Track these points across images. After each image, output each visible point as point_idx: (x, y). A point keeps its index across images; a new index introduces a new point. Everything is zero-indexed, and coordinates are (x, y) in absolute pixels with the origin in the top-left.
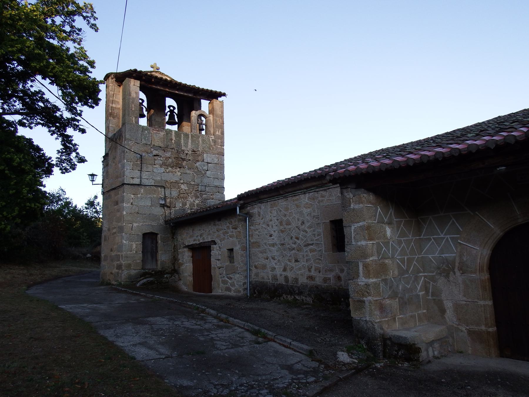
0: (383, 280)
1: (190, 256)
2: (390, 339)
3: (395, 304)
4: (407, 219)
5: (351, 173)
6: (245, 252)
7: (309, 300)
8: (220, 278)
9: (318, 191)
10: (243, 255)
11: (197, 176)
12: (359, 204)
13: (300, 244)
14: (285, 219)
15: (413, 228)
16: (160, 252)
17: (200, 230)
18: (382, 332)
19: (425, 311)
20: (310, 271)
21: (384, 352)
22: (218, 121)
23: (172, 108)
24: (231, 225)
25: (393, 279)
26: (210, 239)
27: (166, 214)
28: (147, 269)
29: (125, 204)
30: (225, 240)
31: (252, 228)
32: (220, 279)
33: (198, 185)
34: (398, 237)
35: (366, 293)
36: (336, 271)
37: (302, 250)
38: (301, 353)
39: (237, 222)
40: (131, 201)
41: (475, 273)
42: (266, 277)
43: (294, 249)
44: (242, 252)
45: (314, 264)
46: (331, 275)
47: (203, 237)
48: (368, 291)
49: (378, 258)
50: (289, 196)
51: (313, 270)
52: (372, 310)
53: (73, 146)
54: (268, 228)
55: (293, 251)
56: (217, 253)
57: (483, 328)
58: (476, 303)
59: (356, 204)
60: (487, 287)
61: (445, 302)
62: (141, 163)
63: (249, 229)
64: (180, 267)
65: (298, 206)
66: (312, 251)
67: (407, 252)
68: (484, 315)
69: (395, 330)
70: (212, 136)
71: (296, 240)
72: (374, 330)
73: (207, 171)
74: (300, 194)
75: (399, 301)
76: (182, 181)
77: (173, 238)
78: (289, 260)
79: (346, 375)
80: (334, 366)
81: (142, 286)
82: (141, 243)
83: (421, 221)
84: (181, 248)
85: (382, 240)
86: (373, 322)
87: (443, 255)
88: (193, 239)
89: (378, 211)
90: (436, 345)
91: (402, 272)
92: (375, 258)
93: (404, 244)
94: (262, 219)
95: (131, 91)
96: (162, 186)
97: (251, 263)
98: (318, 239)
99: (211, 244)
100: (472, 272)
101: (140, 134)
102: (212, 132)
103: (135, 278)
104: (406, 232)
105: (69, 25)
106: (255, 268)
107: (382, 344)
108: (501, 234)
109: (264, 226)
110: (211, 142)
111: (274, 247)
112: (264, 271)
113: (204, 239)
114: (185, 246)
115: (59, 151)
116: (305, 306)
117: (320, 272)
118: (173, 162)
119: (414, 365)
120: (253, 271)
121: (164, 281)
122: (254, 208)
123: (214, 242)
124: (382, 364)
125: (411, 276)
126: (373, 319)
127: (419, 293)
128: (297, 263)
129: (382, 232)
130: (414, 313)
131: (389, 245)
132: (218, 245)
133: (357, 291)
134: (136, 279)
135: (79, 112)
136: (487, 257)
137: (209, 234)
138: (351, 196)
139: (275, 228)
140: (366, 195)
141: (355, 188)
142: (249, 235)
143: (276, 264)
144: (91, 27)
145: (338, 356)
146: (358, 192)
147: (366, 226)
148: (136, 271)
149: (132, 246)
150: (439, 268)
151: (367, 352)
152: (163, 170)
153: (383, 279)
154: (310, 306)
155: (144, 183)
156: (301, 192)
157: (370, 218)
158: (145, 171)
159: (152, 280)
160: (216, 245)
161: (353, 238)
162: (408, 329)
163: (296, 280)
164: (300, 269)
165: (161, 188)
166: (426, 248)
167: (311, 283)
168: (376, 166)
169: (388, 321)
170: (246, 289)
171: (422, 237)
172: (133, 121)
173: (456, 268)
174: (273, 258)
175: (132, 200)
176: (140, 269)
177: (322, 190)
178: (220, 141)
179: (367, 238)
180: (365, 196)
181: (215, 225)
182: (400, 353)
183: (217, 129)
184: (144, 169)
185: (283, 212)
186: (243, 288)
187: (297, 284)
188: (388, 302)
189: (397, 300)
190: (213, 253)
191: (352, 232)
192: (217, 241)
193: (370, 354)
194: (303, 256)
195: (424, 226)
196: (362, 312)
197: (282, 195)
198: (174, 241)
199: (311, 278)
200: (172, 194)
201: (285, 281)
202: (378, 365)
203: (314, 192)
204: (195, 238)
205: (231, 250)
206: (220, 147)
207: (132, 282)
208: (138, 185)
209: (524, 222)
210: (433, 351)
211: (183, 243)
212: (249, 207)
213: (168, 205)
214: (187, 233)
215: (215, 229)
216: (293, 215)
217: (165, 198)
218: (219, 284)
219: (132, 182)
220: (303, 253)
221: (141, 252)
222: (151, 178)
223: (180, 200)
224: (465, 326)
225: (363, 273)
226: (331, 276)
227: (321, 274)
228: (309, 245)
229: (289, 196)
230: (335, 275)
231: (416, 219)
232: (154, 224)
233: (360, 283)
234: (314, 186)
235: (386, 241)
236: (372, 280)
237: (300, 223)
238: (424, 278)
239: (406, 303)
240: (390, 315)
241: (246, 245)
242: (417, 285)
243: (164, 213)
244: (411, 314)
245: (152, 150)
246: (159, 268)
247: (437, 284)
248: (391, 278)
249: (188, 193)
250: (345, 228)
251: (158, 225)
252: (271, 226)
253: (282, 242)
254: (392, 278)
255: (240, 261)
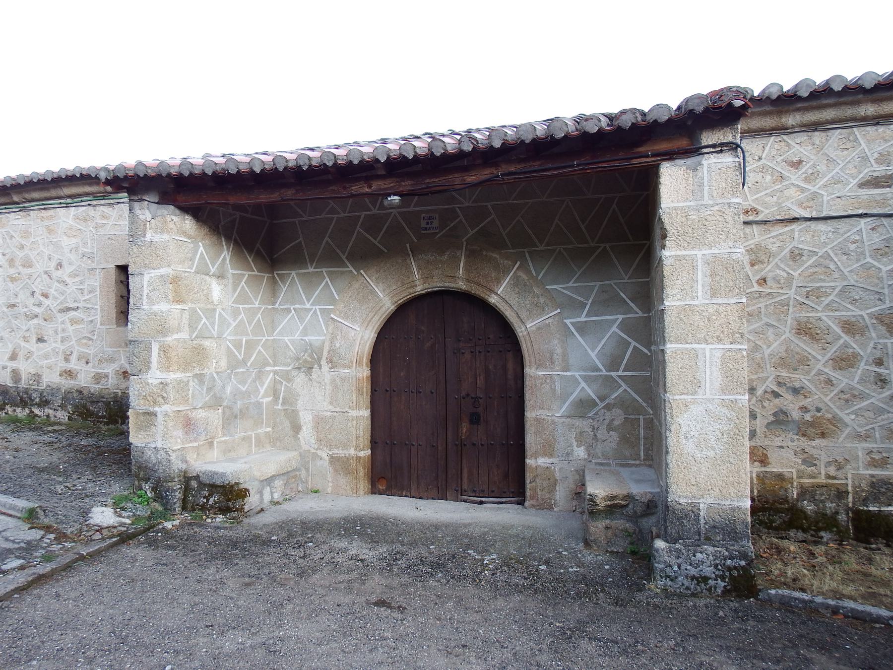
0: (195, 376)
2: (197, 478)
3: (215, 417)
4: (254, 273)
5: (149, 171)
7: (62, 416)
9: (95, 206)
12: (162, 232)
13: (51, 306)
14: (21, 255)
15: (262, 290)
18: (184, 467)
19: (268, 429)
20: (67, 360)
21: (184, 501)
25: (215, 375)
34: (233, 301)
35: (160, 399)
36: (121, 360)
37: (54, 319)
38: (10, 516)
41: (349, 367)
43: (36, 316)
45: (77, 348)
46: (110, 369)
48: (165, 395)
49: (191, 336)
50: (32, 208)
51: (73, 359)
52: (168, 430)
55: (35, 321)
57: (352, 452)
58: (346, 414)
59: (155, 232)
60: (365, 389)
61: (301, 414)
65: (50, 231)
66: (73, 321)
67: (247, 329)
68: (355, 432)
69: (209, 463)
71: (42, 299)
72: (168, 464)
74: (57, 206)
75: (224, 413)
78: (24, 337)
79: (96, 548)
80: (76, 535)
83: (278, 279)
85: (203, 305)
86: (168, 450)
87: (306, 338)
89: (200, 252)
90: (278, 483)
91: (234, 364)
92: (184, 335)
93: (243, 315)
98: (89, 300)
100: (345, 366)
104: (250, 294)
107: (182, 487)
108: (393, 307)
116: (50, 428)
117: (87, 363)
119: (234, 518)
124: (177, 522)
125: (251, 370)
126: (169, 446)
127: (261, 400)
128: (41, 345)
129: (203, 290)
130: (250, 433)
131: (215, 315)
133: (145, 396)
136: (369, 342)
138: (148, 216)
140: (176, 218)
141: (158, 203)
145: (93, 516)
146: (163, 211)
147: (171, 276)
150: (297, 359)
151: (154, 504)
153: (197, 374)
154: (63, 428)
156: (60, 203)
157: (182, 262)
161: (145, 297)
162: (233, 460)
163: (37, 377)
164: (46, 356)
166: (281, 326)
167: (67, 384)
168: (195, 165)
169: (198, 447)
171: (277, 306)
173: (324, 358)
177: (104, 205)
179: (171, 297)
180: (175, 220)
182: (211, 501)
185: (17, 239)
187: (38, 386)
188: (201, 414)
189: (220, 411)
191: (145, 286)
193: (158, 507)
194: (56, 332)
195: (282, 287)
196: (151, 433)
197: (18, 203)
199: (69, 374)
201: (12, 379)
202: (169, 525)
203: (86, 206)
209: (423, 292)
210: (272, 493)
216: (39, 248)
220: (56, 325)
224: (328, 451)
225: (159, 363)
226: (110, 371)
227: (89, 367)
228: (69, 309)
229: (32, 208)
230: (118, 369)
231: (271, 275)
233: (150, 381)
234: (87, 194)
235: (209, 306)
236: (173, 376)
237: (53, 264)
238: (274, 375)
239: (236, 417)
240: (203, 437)
242: (259, 386)
244: (242, 434)
247: (292, 385)
248: (211, 373)
250: (132, 276)
253: (12, 301)
254: (214, 373)
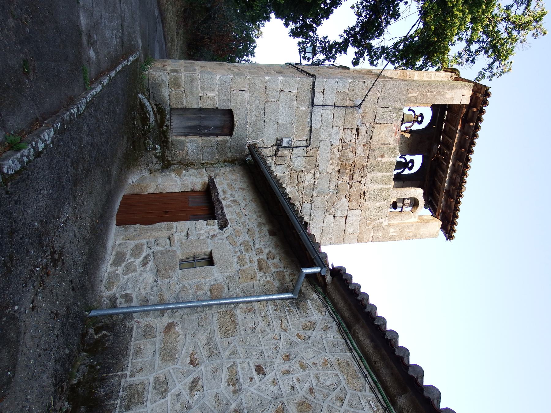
1: (194, 187)
6: (209, 293)
8: (148, 240)
10: (201, 289)
11: (326, 199)
16: (200, 139)
17: (245, 199)
22: (410, 231)
23: (410, 165)
24: (265, 257)
26: (230, 217)
27: (264, 149)
28: (172, 118)
29: (282, 78)
30: (231, 246)
31: (270, 308)
32: (144, 241)
33: (312, 202)
39: (275, 270)
40: (286, 90)
42: (139, 362)
44: (206, 288)
47: (232, 205)
53: (334, 55)
54: (279, 360)
56: (202, 232)
62: (346, 107)
63: (267, 300)
64: (174, 172)
70: (387, 221)
73: (334, 217)
76: (317, 175)
77: (225, 161)
81: (138, 102)
82: (217, 106)
84: (209, 173)
88: (226, 189)
94: (299, 336)
95: (455, 91)
96: (310, 143)
97: (181, 312)
99: (219, 219)
101: (392, 105)
102: (392, 222)
103: (155, 96)
105: (479, 48)
106: (166, 324)
109: (282, 343)
110: (378, 221)
111: (229, 385)
112: (157, 355)
113: (229, 206)
114: (213, 177)
115: (325, 38)
118: (348, 159)
120: (159, 319)
121: (148, 142)
122: (320, 312)
123: (224, 225)
132: (220, 233)
134: (154, 97)
135: (375, 62)
137: (239, 215)
139: (285, 383)
142: (251, 302)
143: (178, 396)
144: (480, 73)
148: (167, 98)
149: (210, 91)
152: (336, 143)
155: (315, 112)
158: (335, 114)
159: (149, 121)
160: (219, 229)
165: (307, 140)
170: (114, 306)
172: (411, 93)
174: (194, 385)
175: (289, 90)
176: (172, 104)
178: (381, 235)
181: (260, 225)
183: (398, 230)
184: (339, 112)
186: (118, 295)
190: (202, 223)
192: (228, 231)
198: (219, 163)
200: (298, 158)
204: (229, 192)
205: (210, 261)
206: (371, 236)
207: (148, 90)
208: (313, 102)
211: (217, 175)
212: (319, 297)
213: (280, 153)
214: (236, 180)
215: (252, 226)
217: (291, 147)
218: (134, 238)
219: (318, 90)
221: (200, 106)
222: (324, 123)
223: (288, 173)
232: (249, 128)
241: (224, 295)
243: (266, 146)
245: (367, 125)
246: (173, 138)
249: (298, 187)
251: (247, 135)
252: (286, 367)
255: (185, 283)
